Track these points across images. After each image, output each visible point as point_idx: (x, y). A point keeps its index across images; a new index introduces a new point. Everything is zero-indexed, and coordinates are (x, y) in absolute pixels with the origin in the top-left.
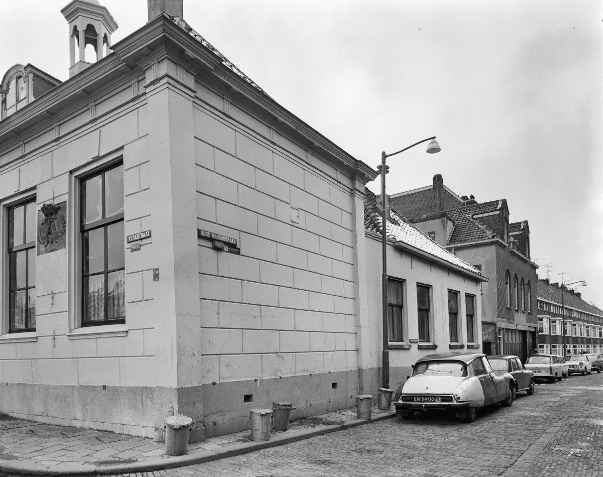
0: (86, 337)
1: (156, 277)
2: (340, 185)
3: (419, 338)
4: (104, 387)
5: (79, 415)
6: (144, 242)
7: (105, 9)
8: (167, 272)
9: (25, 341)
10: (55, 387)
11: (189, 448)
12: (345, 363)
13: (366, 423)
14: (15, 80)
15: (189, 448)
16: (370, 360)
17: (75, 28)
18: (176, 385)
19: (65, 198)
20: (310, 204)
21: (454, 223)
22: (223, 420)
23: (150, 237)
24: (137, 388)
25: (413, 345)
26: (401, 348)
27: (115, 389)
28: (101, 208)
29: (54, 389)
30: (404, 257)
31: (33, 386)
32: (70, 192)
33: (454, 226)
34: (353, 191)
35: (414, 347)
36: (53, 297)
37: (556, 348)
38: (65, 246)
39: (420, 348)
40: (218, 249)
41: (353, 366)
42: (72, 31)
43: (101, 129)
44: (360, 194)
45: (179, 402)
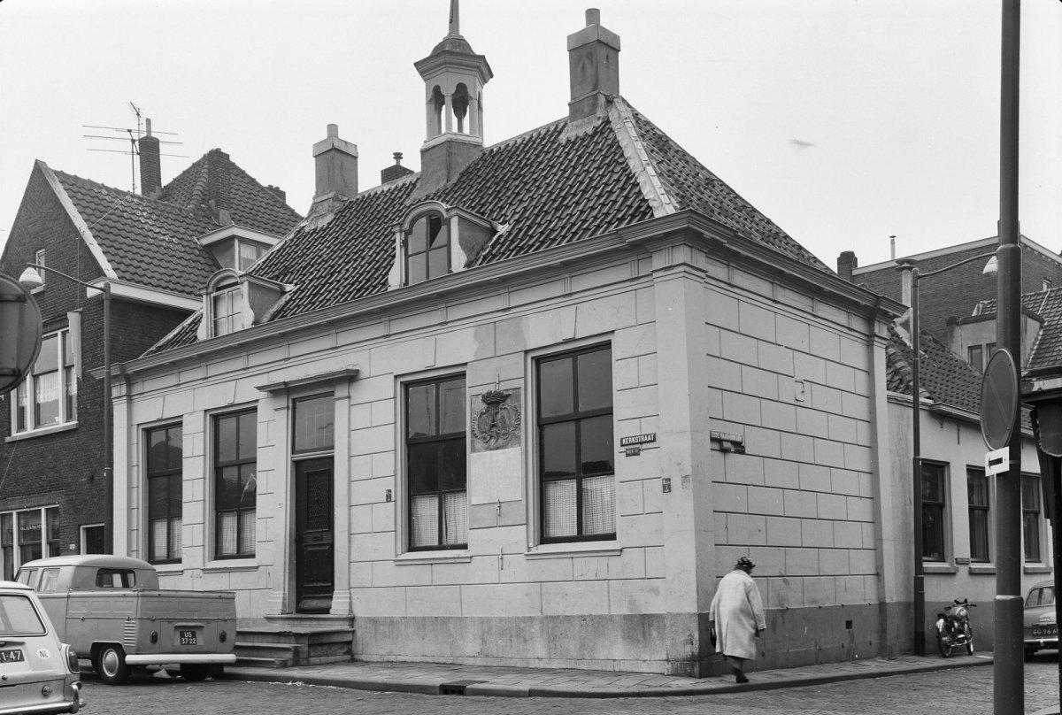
0: (556, 556)
1: (667, 487)
2: (853, 333)
3: (972, 556)
6: (644, 446)
7: (483, 57)
9: (449, 561)
12: (860, 593)
16: (895, 591)
20: (815, 370)
21: (1042, 322)
23: (654, 441)
25: (961, 567)
27: (601, 617)
29: (500, 622)
30: (946, 425)
31: (460, 619)
33: (1041, 328)
34: (870, 339)
35: (963, 570)
36: (500, 507)
37: (89, 552)
39: (972, 573)
40: (724, 451)
41: (871, 598)
42: (431, 94)
43: (579, 305)
44: (880, 340)
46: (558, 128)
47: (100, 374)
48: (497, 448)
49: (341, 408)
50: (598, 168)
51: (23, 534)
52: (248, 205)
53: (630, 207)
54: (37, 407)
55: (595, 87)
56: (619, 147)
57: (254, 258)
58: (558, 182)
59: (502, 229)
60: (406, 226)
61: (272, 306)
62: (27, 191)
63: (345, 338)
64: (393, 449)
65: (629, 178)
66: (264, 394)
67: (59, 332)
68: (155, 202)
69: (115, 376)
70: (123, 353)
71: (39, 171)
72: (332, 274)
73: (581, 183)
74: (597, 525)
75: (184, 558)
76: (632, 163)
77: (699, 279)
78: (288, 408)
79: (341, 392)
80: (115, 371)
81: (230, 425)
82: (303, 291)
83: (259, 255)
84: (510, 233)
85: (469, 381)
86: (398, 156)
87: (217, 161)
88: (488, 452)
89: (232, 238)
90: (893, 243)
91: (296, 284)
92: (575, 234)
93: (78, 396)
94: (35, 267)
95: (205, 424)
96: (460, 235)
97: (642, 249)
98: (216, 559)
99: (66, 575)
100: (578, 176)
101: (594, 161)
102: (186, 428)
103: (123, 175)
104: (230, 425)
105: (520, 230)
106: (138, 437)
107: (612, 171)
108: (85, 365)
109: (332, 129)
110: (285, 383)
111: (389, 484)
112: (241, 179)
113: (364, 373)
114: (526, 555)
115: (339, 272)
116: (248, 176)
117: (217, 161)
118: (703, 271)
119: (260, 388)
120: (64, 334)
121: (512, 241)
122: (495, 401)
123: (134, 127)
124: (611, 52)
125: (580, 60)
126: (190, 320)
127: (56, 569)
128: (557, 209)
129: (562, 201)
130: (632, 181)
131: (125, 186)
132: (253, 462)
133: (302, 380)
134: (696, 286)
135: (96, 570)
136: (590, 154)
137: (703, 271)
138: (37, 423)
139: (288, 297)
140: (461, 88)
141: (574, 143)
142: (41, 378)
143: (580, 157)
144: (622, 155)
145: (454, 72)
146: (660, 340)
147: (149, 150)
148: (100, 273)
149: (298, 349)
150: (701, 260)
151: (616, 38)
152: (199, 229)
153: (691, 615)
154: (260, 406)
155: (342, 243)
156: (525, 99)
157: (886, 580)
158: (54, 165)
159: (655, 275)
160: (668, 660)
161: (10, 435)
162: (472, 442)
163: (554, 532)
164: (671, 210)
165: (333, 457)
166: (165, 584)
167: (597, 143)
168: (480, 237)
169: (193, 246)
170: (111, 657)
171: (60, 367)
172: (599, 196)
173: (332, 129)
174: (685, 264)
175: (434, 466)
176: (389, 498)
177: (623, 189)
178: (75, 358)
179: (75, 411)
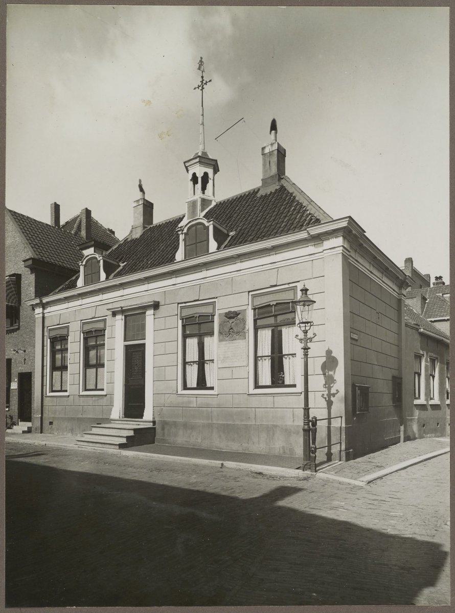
46: (255, 192)
110: (122, 308)
113: (162, 303)
122: (232, 316)
131: (49, 223)
140: (206, 174)
147: (56, 208)
163: (189, 386)
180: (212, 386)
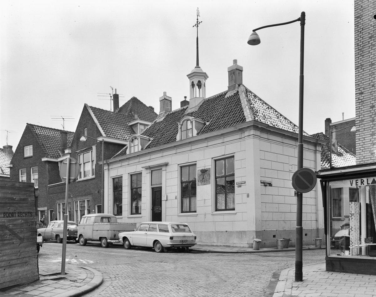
1: (248, 196)
4: (226, 231)
5: (215, 241)
6: (243, 184)
7: (205, 73)
8: (252, 195)
10: (205, 232)
11: (260, 249)
13: (319, 249)
14: (186, 121)
15: (260, 249)
17: (193, 82)
18: (255, 230)
19: (210, 167)
22: (267, 243)
24: (240, 231)
26: (339, 220)
27: (231, 232)
28: (224, 171)
32: (212, 165)
34: (315, 151)
37: (98, 213)
38: (210, 184)
40: (265, 186)
45: (256, 235)
46: (222, 96)
47: (101, 163)
48: (204, 185)
49: (164, 173)
50: (234, 106)
51: (81, 207)
52: (143, 113)
53: (240, 118)
54: (85, 172)
55: (235, 82)
56: (240, 100)
57: (143, 129)
58: (223, 110)
59: (208, 124)
60: (181, 123)
61: (146, 144)
62: (82, 112)
63: (165, 154)
64: (167, 187)
65: (241, 109)
66: (144, 169)
67: (90, 151)
68: (117, 114)
69: (105, 164)
70: (107, 157)
71: (86, 107)
72: (163, 135)
73: (229, 110)
74: (230, 206)
75: (236, 207)
76: (242, 105)
77: (258, 139)
78: (150, 173)
79: (164, 168)
80: (105, 162)
81: (136, 178)
82: (155, 140)
83: (145, 128)
84: (209, 124)
85: (197, 166)
86: (185, 97)
87: (134, 100)
88: (202, 186)
89: (138, 123)
90: (343, 115)
91: (153, 138)
92: (226, 125)
93: (95, 169)
94: (84, 136)
95: (128, 177)
96: (195, 126)
97: (242, 130)
98: (131, 214)
99: (93, 219)
100: (229, 108)
101: (233, 104)
102: (123, 178)
103: (108, 106)
104: (136, 178)
105: (212, 124)
106: (111, 181)
107: (237, 107)
108: (97, 161)
109: (165, 93)
110: (149, 166)
111: (176, 194)
112: (141, 105)
114: (178, 215)
115: (165, 135)
116: (143, 104)
117: (134, 100)
118: (259, 136)
119: (143, 168)
120: (92, 152)
121: (210, 127)
122: (204, 172)
123: (111, 93)
124: (240, 72)
125: (231, 74)
126: (125, 148)
127: (90, 217)
128: (222, 118)
129: (223, 116)
130: (242, 110)
131: (108, 109)
132: (141, 187)
133: (154, 165)
134: (257, 141)
135: (100, 218)
136: (232, 101)
137: (259, 136)
138: (85, 176)
139: (151, 141)
140: (199, 82)
141: (229, 98)
142: (86, 164)
143: (230, 102)
144: (240, 102)
145: (198, 79)
146: (247, 155)
147: (116, 98)
148: (101, 135)
149: (153, 156)
150: (258, 133)
151: (242, 68)
152: (129, 120)
153: (253, 231)
154: (143, 172)
155: (166, 126)
156: (217, 85)
157: (319, 222)
158: (89, 105)
159: (246, 137)
160: (248, 244)
161: (77, 180)
162: (198, 183)
163: (133, 213)
164: (251, 119)
165: (161, 187)
166: (119, 221)
167: (234, 98)
168: (201, 126)
169: (127, 125)
170: (104, 241)
171: (90, 161)
172: (233, 114)
173: (165, 93)
174: (253, 135)
175: (188, 190)
176: (176, 198)
177: (239, 112)
178: (95, 158)
179: (94, 173)
180: (195, 210)
